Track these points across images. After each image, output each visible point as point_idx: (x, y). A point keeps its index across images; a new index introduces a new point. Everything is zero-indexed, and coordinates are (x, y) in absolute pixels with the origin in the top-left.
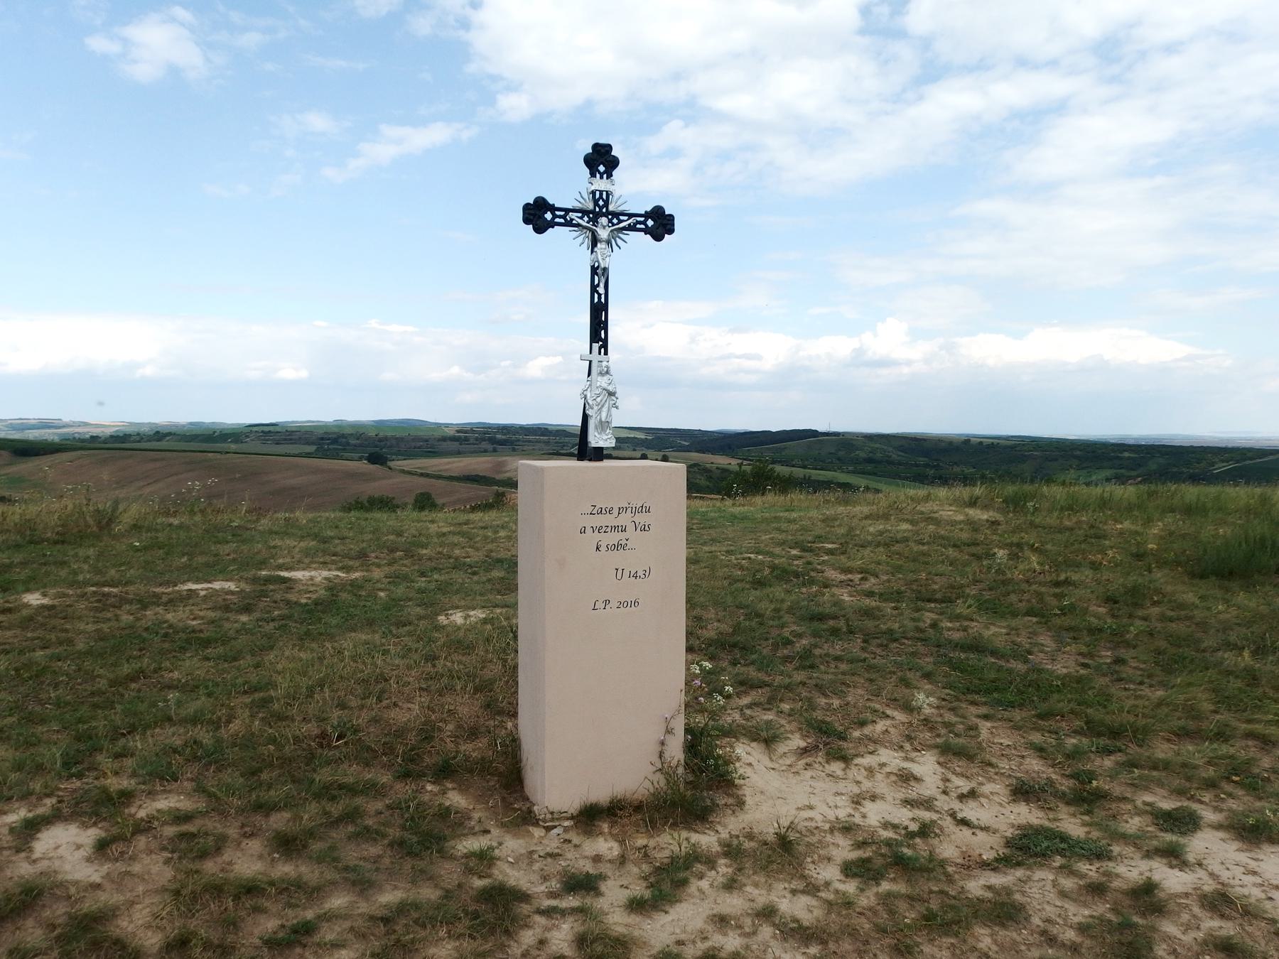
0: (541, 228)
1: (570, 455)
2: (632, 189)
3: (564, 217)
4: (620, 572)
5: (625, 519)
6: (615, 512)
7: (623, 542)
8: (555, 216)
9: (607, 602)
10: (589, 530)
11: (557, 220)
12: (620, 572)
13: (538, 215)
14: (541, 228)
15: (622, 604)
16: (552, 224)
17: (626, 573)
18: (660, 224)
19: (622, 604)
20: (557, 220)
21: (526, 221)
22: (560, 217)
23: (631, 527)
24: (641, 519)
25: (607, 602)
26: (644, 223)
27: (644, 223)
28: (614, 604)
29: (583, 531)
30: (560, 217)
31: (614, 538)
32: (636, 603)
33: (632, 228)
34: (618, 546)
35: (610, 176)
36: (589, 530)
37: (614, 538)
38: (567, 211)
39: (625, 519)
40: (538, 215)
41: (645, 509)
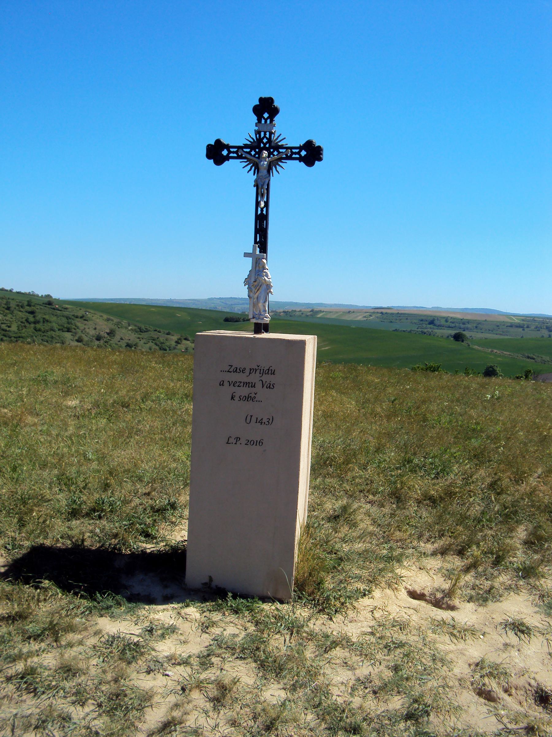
0: (309, 145)
1: (251, 331)
2: (289, 131)
3: (236, 152)
4: (249, 418)
5: (255, 378)
6: (247, 371)
7: (253, 395)
8: (230, 152)
9: (238, 439)
10: (226, 384)
11: (231, 155)
12: (249, 418)
13: (217, 153)
14: (309, 145)
15: (249, 442)
16: (227, 158)
17: (254, 419)
18: (311, 154)
19: (249, 442)
20: (231, 155)
21: (209, 156)
22: (233, 152)
23: (259, 385)
24: (267, 378)
25: (238, 439)
26: (299, 153)
27: (299, 153)
28: (243, 441)
29: (222, 384)
30: (233, 152)
31: (245, 391)
32: (261, 443)
33: (289, 158)
34: (248, 398)
35: (272, 121)
36: (226, 384)
37: (245, 391)
38: (239, 148)
39: (255, 378)
40: (217, 153)
41: (271, 372)
